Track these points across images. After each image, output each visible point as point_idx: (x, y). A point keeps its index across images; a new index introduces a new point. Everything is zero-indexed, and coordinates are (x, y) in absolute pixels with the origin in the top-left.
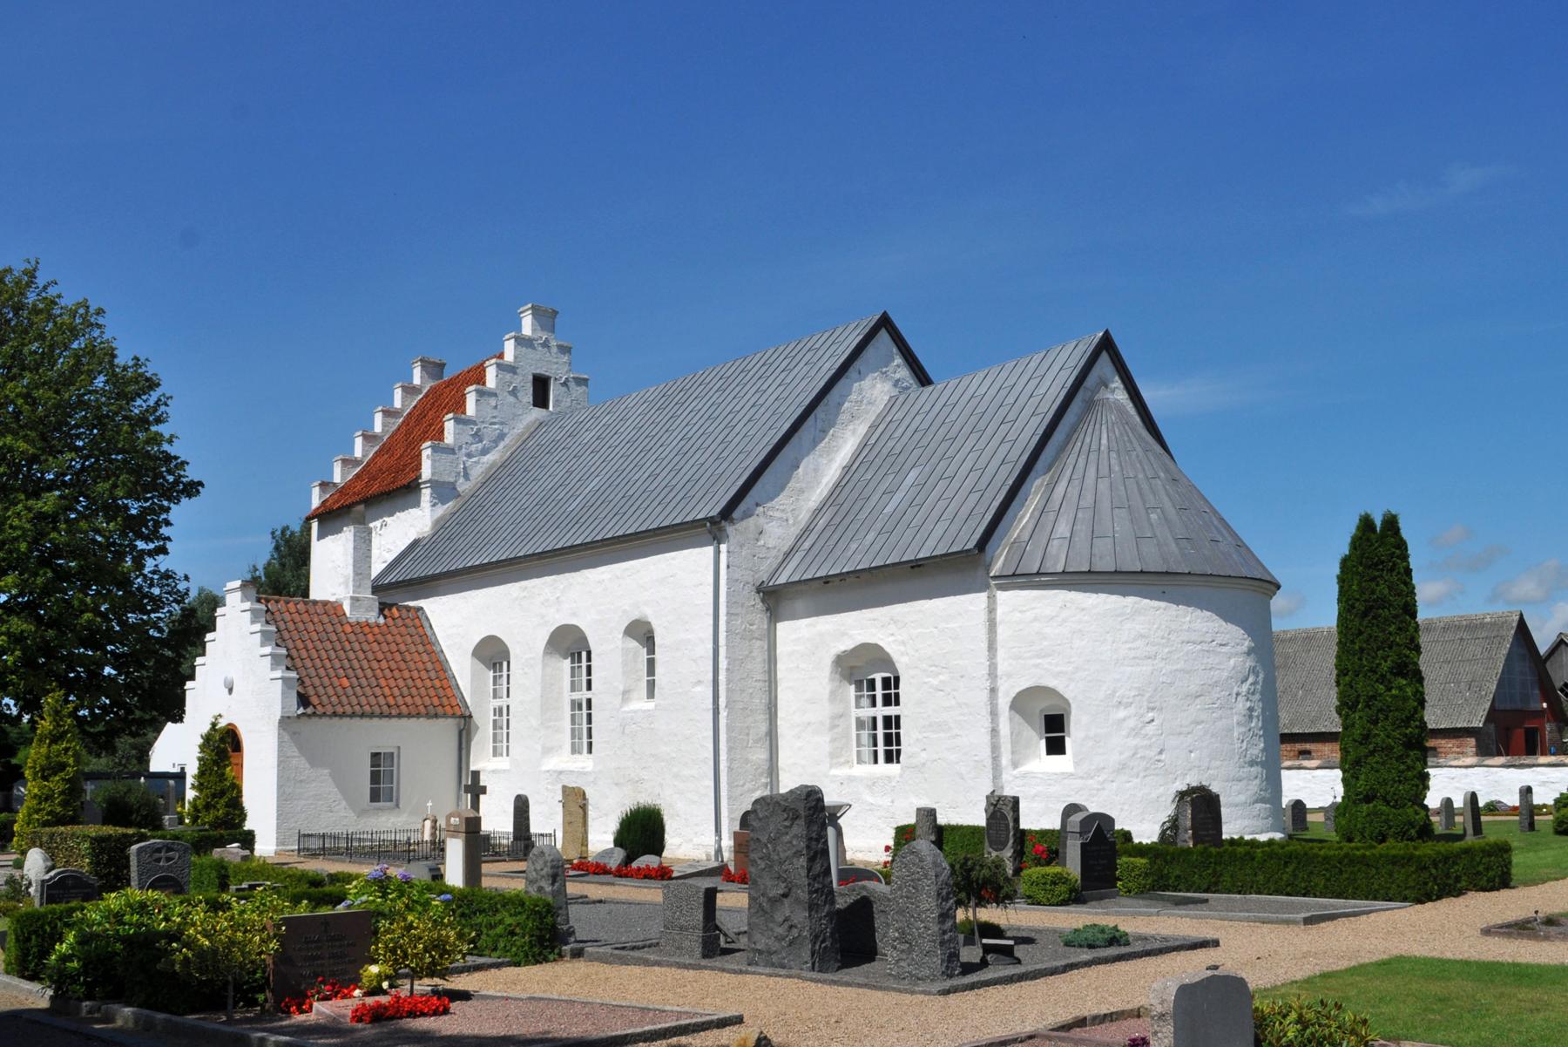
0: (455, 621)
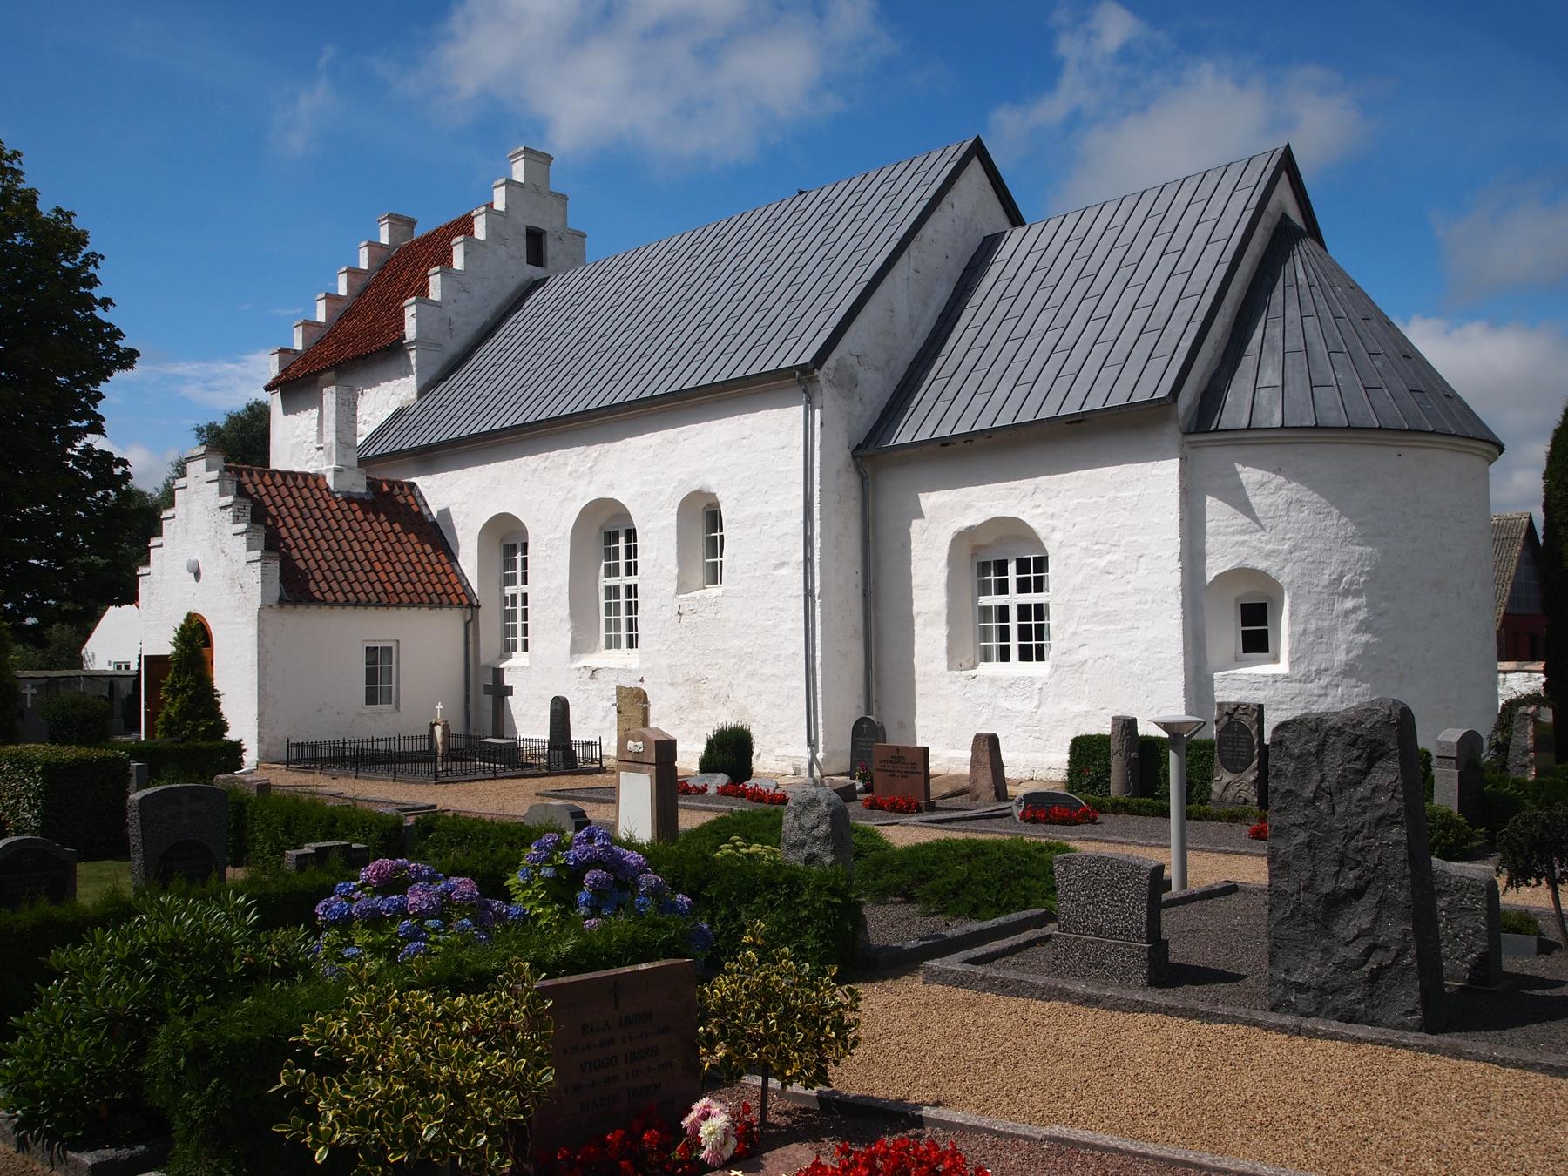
0: (461, 497)
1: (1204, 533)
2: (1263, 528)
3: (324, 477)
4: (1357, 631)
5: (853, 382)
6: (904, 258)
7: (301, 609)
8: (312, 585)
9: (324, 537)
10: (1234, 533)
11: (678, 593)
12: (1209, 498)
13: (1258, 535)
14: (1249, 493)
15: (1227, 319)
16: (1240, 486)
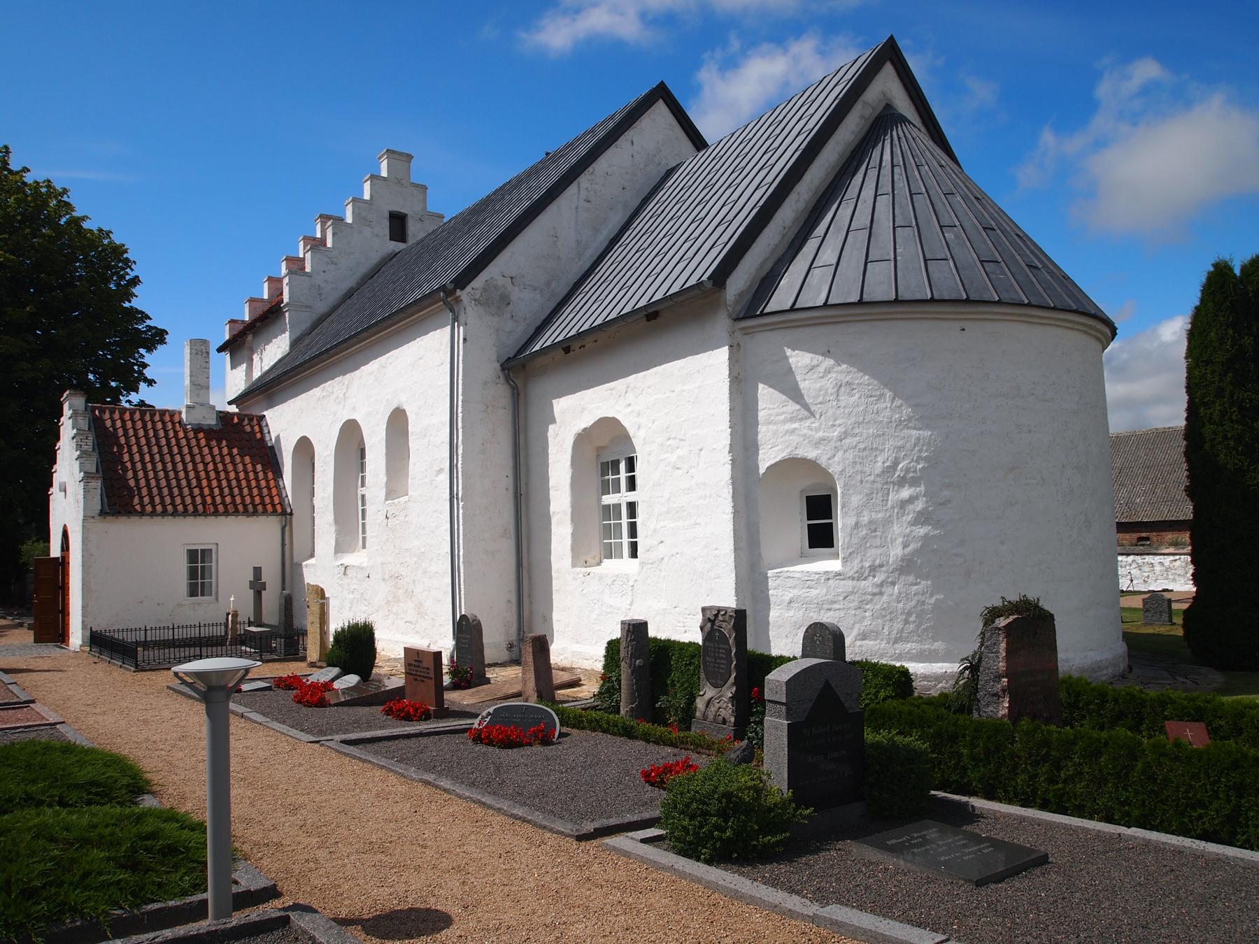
0: (285, 423)
1: (757, 423)
2: (812, 414)
3: (180, 413)
4: (914, 523)
5: (505, 300)
6: (572, 190)
7: (123, 519)
8: (136, 500)
9: (206, 465)
10: (784, 422)
11: (386, 499)
12: (761, 386)
13: (808, 423)
14: (798, 378)
15: (801, 205)
16: (790, 371)
